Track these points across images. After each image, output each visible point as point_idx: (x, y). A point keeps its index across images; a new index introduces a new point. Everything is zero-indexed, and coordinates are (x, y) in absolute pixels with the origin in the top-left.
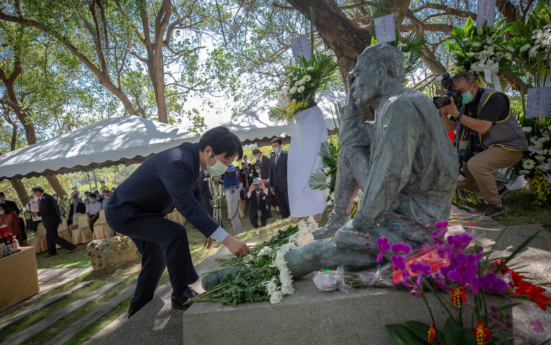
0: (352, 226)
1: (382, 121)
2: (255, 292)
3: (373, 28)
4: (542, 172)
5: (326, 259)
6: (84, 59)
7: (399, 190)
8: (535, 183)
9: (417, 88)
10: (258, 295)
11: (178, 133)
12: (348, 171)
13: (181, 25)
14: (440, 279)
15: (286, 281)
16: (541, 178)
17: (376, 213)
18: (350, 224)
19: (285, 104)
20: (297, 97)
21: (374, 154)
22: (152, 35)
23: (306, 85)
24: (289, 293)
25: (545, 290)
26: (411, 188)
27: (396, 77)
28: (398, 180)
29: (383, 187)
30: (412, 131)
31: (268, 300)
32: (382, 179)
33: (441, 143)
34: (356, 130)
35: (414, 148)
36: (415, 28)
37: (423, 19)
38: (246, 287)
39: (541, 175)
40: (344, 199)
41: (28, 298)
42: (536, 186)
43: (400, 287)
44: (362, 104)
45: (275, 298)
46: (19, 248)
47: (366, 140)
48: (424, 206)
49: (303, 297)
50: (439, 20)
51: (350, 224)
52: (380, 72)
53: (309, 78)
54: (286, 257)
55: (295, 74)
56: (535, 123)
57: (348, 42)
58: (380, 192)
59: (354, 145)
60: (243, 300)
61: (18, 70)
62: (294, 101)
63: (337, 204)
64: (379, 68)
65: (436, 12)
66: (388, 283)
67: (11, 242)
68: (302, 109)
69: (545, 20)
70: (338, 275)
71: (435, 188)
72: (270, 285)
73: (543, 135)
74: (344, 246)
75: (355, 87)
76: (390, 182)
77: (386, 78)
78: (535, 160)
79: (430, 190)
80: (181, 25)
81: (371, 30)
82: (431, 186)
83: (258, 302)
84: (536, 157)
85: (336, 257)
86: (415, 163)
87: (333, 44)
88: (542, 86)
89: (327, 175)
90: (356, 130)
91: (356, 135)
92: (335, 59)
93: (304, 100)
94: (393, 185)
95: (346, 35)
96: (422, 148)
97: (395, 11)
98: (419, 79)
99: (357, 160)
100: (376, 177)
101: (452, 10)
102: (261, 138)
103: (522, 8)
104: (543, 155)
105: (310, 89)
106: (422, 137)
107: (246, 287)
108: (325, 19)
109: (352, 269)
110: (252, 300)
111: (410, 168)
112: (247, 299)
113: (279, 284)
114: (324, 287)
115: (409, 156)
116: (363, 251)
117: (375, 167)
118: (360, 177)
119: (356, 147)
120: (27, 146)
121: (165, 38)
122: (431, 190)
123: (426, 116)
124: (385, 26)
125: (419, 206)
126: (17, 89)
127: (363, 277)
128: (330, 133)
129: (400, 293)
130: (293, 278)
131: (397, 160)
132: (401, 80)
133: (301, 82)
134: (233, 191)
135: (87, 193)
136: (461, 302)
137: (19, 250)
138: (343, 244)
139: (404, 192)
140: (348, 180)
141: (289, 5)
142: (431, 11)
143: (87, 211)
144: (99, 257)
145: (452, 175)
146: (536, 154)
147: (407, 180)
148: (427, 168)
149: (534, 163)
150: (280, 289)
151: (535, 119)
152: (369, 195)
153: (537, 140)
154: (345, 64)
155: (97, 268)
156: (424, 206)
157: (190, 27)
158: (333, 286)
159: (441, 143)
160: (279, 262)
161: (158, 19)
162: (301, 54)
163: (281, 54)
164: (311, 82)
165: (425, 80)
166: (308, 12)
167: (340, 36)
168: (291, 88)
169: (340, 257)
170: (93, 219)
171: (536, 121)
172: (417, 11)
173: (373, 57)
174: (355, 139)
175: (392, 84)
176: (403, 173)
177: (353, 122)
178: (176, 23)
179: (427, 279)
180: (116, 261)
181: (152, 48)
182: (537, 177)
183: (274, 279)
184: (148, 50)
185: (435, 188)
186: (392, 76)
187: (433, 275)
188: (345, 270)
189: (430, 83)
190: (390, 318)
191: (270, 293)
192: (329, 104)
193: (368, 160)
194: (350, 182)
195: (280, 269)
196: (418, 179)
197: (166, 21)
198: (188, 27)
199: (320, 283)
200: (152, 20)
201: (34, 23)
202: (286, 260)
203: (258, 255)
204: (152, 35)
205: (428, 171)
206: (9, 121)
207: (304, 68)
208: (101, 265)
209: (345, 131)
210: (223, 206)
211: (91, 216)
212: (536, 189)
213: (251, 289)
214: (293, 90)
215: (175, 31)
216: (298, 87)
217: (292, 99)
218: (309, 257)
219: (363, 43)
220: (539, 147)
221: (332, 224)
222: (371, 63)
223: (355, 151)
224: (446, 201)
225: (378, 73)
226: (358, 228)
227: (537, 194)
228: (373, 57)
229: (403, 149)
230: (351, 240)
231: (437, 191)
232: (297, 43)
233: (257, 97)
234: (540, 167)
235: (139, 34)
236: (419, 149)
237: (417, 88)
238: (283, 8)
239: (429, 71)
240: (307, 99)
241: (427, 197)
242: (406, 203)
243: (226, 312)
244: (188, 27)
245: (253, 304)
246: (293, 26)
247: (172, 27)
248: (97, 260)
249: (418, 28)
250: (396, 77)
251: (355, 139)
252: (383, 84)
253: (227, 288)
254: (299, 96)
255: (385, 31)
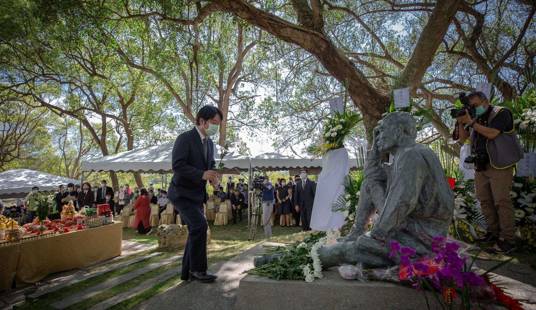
0: (370, 236)
1: (398, 164)
2: (295, 272)
3: (392, 96)
4: (532, 222)
5: (349, 256)
6: (177, 96)
7: (408, 213)
8: (526, 230)
9: (424, 142)
10: (297, 274)
11: (233, 156)
12: (368, 196)
13: (245, 79)
14: (436, 280)
15: (318, 268)
16: (531, 227)
17: (389, 228)
18: (368, 234)
19: (321, 143)
20: (330, 139)
21: (390, 186)
22: (225, 85)
23: (338, 132)
24: (319, 277)
25: (522, 305)
26: (417, 213)
27: (409, 135)
28: (408, 206)
29: (396, 209)
30: (419, 173)
31: (304, 280)
32: (396, 203)
33: (441, 184)
34: (377, 168)
35: (421, 185)
36: (425, 96)
37: (432, 89)
38: (287, 268)
39: (531, 225)
40: (363, 217)
41: (111, 259)
42: (526, 233)
43: (405, 283)
44: (383, 150)
45: (309, 278)
46: (113, 221)
47: (384, 176)
48: (426, 229)
49: (330, 281)
50: (446, 92)
51: (368, 234)
52: (399, 130)
53: (341, 127)
54: (319, 251)
55: (330, 123)
56: (525, 180)
57: (372, 104)
58: (393, 213)
59: (374, 178)
60: (284, 276)
61: (132, 100)
62: (328, 142)
63: (357, 220)
64: (397, 128)
65: (443, 85)
66: (396, 279)
67: (109, 216)
68: (333, 149)
69: (533, 102)
70: (358, 269)
71: (435, 216)
72: (306, 269)
73: (532, 191)
74: (364, 248)
75: (379, 138)
76: (401, 206)
77: (403, 134)
78: (525, 211)
79: (431, 217)
80: (245, 79)
81: (390, 97)
82: (432, 214)
83: (296, 279)
84: (526, 208)
85: (357, 256)
86: (421, 196)
87: (361, 104)
88: (531, 152)
89: (347, 201)
90: (377, 168)
91: (376, 171)
92: (361, 116)
93: (335, 141)
94: (403, 209)
95: (371, 99)
96: (427, 186)
97: (410, 85)
98: (427, 135)
99: (376, 189)
100: (391, 202)
101: (457, 85)
102: (294, 167)
103: (519, 88)
104: (532, 208)
105: (340, 135)
106: (427, 178)
107: (287, 268)
108: (356, 87)
109: (368, 266)
110: (291, 278)
111: (417, 199)
112: (288, 277)
113: (312, 269)
114: (346, 276)
115: (417, 190)
116: (378, 254)
117: (391, 195)
118: (377, 203)
119: (376, 180)
120: (127, 152)
121: (233, 87)
122: (432, 217)
123: (431, 164)
124: (402, 96)
125: (422, 228)
126: (129, 112)
127: (376, 273)
128: (354, 169)
129: (404, 288)
130: (322, 267)
131: (408, 191)
132: (413, 137)
133: (335, 129)
134: (268, 205)
135: (159, 190)
136: (451, 299)
137: (113, 223)
138: (363, 246)
139: (411, 216)
140: (367, 203)
141: (327, 72)
142: (439, 85)
143: (158, 203)
144: (165, 238)
145: (449, 208)
146: (526, 206)
147: (414, 207)
148: (430, 201)
149: (525, 213)
150: (312, 273)
151: (525, 177)
152: (385, 214)
153: (527, 195)
154: (368, 119)
155: (162, 246)
156: (426, 229)
157: (251, 81)
158: (353, 276)
159: (441, 184)
160: (313, 254)
161: (230, 74)
162: (336, 110)
163: (316, 106)
164: (342, 130)
165: (432, 136)
166: (344, 81)
167: (366, 99)
168: (326, 132)
169: (359, 256)
170: (162, 209)
171: (527, 180)
172: (427, 83)
173: (394, 120)
174: (376, 175)
175: (407, 139)
176: (412, 201)
177: (375, 162)
178: (243, 78)
179: (426, 279)
180: (176, 243)
181: (222, 92)
182: (527, 225)
183: (309, 265)
184: (220, 95)
185: (435, 216)
186: (407, 134)
187: (431, 277)
188: (363, 266)
189: (436, 139)
190: (395, 306)
191: (305, 274)
192: (354, 148)
193: (385, 191)
194: (369, 205)
195: (313, 259)
196: (423, 208)
197: (236, 76)
198: (249, 81)
199: (344, 272)
200: (226, 75)
201: (151, 71)
202: (318, 253)
203: (298, 247)
204: (225, 85)
205: (430, 203)
206: (118, 132)
207: (337, 119)
208: (165, 244)
209: (368, 168)
210: (259, 215)
211: (160, 207)
212: (526, 235)
213: (292, 270)
214: (327, 135)
215: (241, 83)
216: (332, 132)
217: (326, 140)
218: (337, 253)
219: (383, 106)
220: (528, 201)
221: (353, 235)
222: (392, 123)
223: (375, 183)
224: (443, 227)
225: (397, 131)
226: (373, 237)
227: (527, 240)
228: (394, 120)
229: (413, 185)
230: (369, 245)
231: (437, 218)
232: (333, 103)
233: (293, 135)
234: (531, 217)
235: (215, 82)
236: (425, 186)
237: (424, 142)
238: (322, 74)
239: (435, 130)
240: (338, 141)
241: (429, 222)
242: (412, 224)
243: (272, 283)
244: (249, 81)
245: (292, 281)
246: (327, 87)
247: (240, 80)
248: (163, 240)
249: (428, 96)
250: (409, 135)
251: (376, 175)
252: (400, 139)
253: (274, 267)
254: (332, 139)
255: (402, 99)
